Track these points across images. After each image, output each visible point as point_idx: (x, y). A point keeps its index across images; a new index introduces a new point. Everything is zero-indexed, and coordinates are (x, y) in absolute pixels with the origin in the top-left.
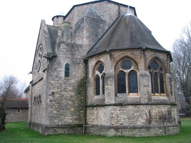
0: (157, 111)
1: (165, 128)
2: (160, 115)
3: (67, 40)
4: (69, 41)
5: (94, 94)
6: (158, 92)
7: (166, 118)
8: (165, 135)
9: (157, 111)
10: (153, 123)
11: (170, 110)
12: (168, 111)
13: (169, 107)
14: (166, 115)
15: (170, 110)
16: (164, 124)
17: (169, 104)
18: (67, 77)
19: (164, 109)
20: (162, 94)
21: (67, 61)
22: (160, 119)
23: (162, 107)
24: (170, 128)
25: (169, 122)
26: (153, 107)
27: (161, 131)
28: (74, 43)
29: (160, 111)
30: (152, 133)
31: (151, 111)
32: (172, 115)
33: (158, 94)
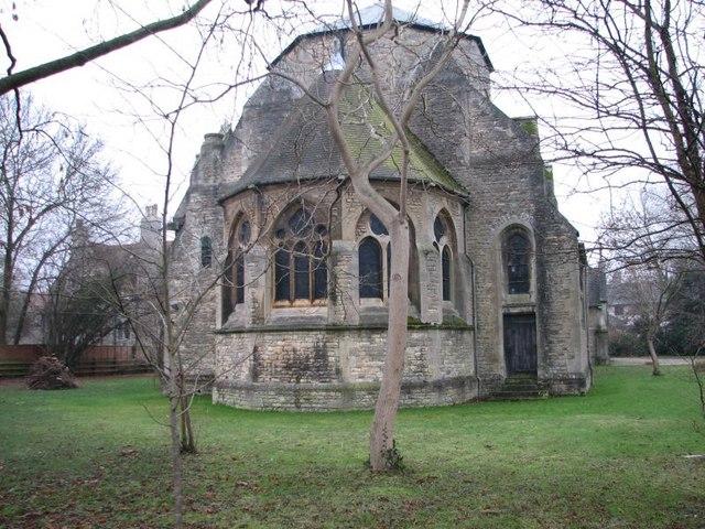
0: (278, 349)
1: (297, 392)
2: (289, 360)
3: (206, 180)
4: (211, 182)
5: (508, 306)
6: (307, 297)
7: (307, 368)
8: (295, 410)
9: (278, 349)
10: (265, 378)
11: (325, 346)
12: (317, 349)
13: (320, 336)
14: (307, 358)
15: (325, 346)
16: (298, 382)
17: (320, 330)
18: (518, 292)
19: (303, 344)
20: (317, 301)
21: (207, 231)
22: (288, 367)
23: (295, 337)
24: (314, 393)
25: (319, 377)
26: (268, 337)
27: (282, 399)
28: (220, 184)
29: (290, 348)
30: (258, 401)
31: (468, 336)
32: (331, 359)
33: (306, 302)
